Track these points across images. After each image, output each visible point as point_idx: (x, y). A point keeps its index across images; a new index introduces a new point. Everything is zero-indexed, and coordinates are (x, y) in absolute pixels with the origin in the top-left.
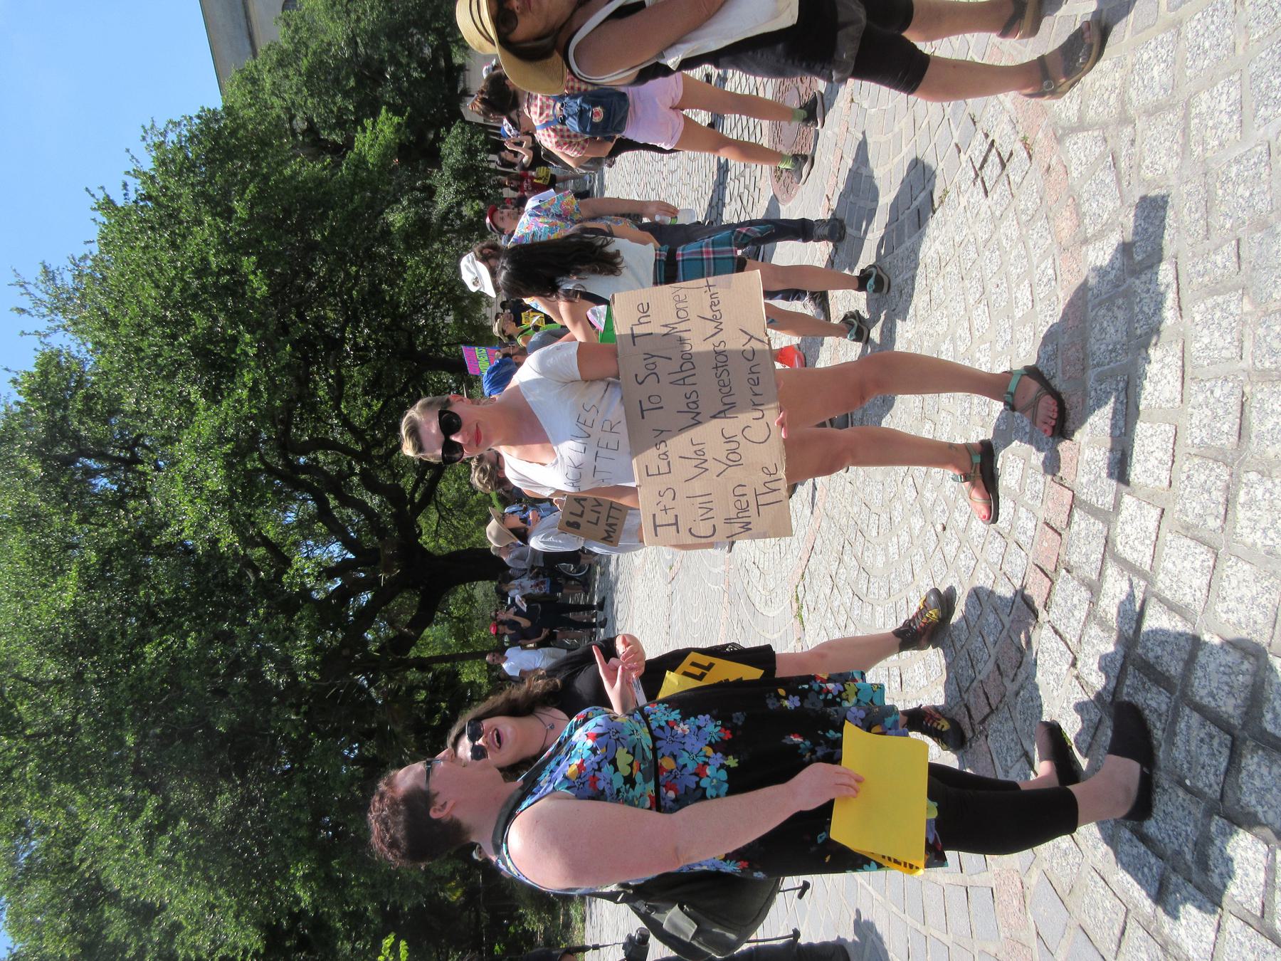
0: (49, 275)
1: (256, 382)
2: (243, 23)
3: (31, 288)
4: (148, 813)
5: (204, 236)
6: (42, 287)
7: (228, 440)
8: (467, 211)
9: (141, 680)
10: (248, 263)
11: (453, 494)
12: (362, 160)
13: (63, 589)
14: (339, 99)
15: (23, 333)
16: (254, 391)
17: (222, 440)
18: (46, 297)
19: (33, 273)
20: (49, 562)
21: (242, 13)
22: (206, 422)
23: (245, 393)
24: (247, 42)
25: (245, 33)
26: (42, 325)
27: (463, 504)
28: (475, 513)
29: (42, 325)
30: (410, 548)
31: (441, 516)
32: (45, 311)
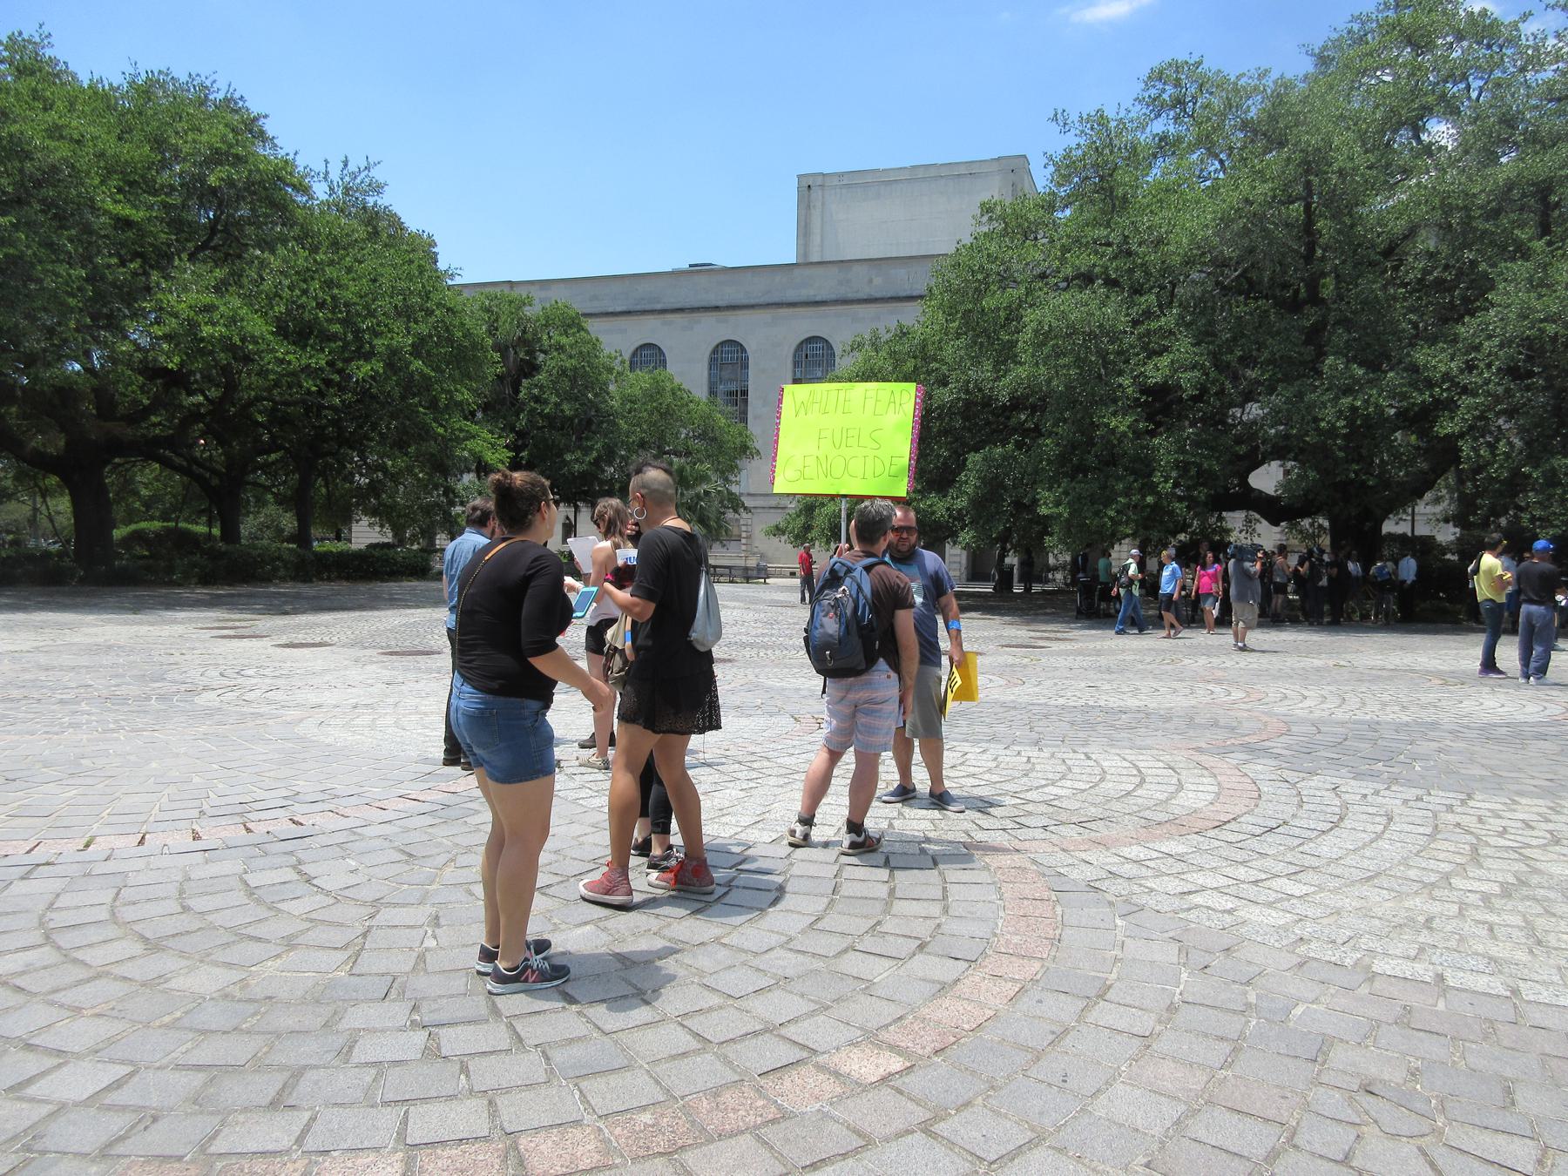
1: (289, 363)
2: (639, 308)
10: (380, 367)
14: (554, 399)
15: (326, 162)
16: (282, 361)
17: (243, 340)
18: (358, 181)
19: (378, 174)
21: (648, 307)
22: (258, 326)
24: (624, 308)
25: (631, 308)
26: (335, 176)
29: (335, 176)
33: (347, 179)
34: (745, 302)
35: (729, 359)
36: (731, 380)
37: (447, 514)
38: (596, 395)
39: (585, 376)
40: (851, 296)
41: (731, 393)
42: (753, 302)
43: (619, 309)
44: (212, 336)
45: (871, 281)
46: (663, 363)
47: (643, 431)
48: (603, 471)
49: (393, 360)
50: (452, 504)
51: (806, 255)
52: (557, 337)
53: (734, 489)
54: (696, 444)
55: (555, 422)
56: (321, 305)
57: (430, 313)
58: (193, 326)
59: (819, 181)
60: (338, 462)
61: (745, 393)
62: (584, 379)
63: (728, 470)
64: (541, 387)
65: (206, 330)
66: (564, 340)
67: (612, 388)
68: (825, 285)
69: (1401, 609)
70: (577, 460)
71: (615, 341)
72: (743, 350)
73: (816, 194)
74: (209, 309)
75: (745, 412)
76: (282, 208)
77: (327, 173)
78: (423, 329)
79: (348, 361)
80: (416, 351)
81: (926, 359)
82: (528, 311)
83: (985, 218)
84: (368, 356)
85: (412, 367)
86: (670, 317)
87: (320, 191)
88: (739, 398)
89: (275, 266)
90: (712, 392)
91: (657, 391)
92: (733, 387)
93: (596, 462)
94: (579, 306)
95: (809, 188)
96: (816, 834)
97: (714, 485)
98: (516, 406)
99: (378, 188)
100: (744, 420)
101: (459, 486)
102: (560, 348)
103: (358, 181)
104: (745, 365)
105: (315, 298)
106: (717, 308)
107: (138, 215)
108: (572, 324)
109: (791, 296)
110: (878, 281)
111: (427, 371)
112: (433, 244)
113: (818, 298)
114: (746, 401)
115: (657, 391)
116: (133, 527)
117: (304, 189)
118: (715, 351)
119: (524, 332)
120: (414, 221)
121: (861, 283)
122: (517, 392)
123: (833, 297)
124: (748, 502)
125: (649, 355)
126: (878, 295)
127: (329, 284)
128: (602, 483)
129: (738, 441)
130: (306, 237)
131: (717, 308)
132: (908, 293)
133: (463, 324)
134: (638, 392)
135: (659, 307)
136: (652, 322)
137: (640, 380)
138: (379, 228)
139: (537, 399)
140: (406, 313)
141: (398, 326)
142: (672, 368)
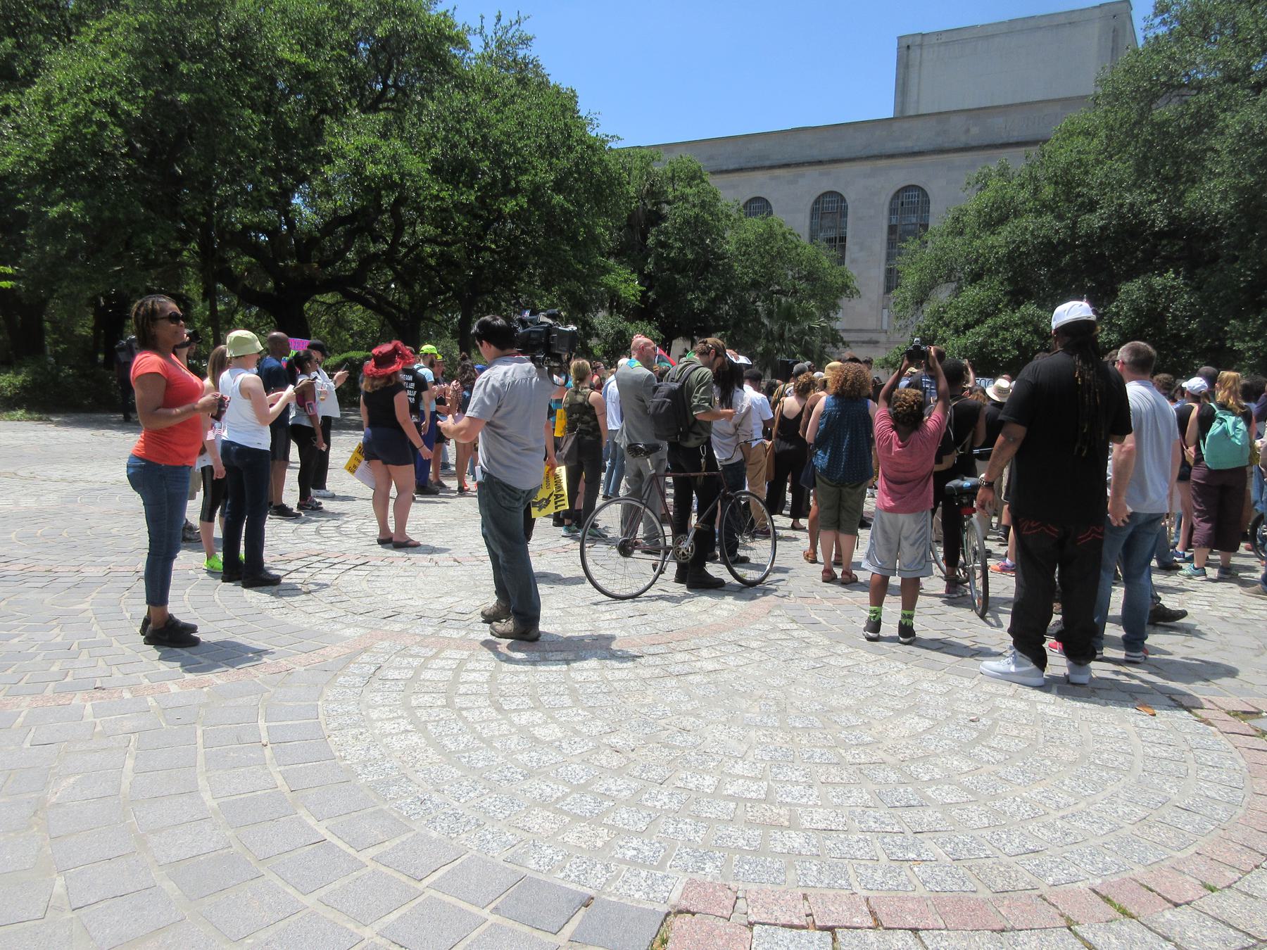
0: (526, 41)
1: (443, 199)
2: (749, 165)
3: (514, 28)
4: (125, 106)
5: (543, 173)
6: (517, 34)
7: (401, 179)
8: (593, 342)
9: (227, 106)
10: (524, 201)
11: (350, 316)
12: (606, 270)
13: (292, 51)
14: (678, 244)
15: (482, 17)
16: (437, 198)
17: (402, 176)
18: (510, 35)
19: (527, 29)
20: (313, 38)
21: (758, 164)
22: (415, 165)
23: (435, 192)
24: (737, 166)
25: (743, 165)
26: (489, 31)
27: (341, 326)
28: (333, 336)
29: (489, 31)
30: (312, 287)
31: (330, 306)
32: (500, 33)
33: (500, 33)
34: (847, 156)
35: (830, 210)
36: (830, 228)
37: (584, 345)
38: (713, 241)
39: (705, 223)
40: (947, 145)
41: (830, 240)
42: (853, 155)
43: (732, 167)
44: (375, 175)
45: (968, 131)
46: (770, 213)
47: (755, 273)
48: (720, 308)
49: (536, 193)
50: (589, 336)
51: (902, 111)
52: (681, 188)
53: (837, 325)
54: (802, 285)
55: (678, 266)
56: (473, 144)
57: (570, 149)
58: (358, 170)
59: (918, 40)
60: (495, 299)
61: (843, 239)
62: (701, 227)
63: (829, 308)
64: (666, 233)
65: (370, 169)
66: (688, 191)
67: (728, 234)
68: (922, 136)
69: (41, 332)
70: (697, 298)
71: (731, 193)
72: (843, 199)
73: (915, 54)
74: (372, 149)
75: (843, 258)
76: (443, 64)
77: (482, 27)
78: (563, 164)
79: (496, 197)
80: (559, 186)
81: (1069, 185)
82: (657, 168)
83: (1158, 20)
84: (514, 193)
85: (554, 202)
86: (778, 172)
87: (476, 44)
88: (839, 242)
89: (433, 108)
90: (812, 238)
91: (768, 237)
92: (832, 234)
93: (713, 301)
94: (698, 163)
95: (908, 49)
96: (883, 632)
97: (818, 322)
98: (644, 252)
99: (526, 41)
100: (841, 261)
101: (596, 321)
102: (684, 198)
103: (510, 35)
104: (843, 213)
105: (467, 137)
106: (820, 162)
107: (315, 66)
108: (694, 177)
109: (890, 147)
110: (975, 130)
111: (566, 205)
112: (573, 97)
113: (916, 149)
114: (843, 247)
115: (768, 237)
116: (344, 355)
117: (460, 42)
118: (817, 201)
119: (652, 185)
120: (559, 74)
121: (958, 132)
122: (645, 238)
123: (931, 147)
124: (846, 337)
125: (758, 206)
126: (974, 144)
127: (480, 124)
128: (717, 319)
129: (840, 281)
130: (463, 83)
131: (820, 162)
132: (1005, 140)
133: (601, 160)
134: (752, 237)
135: (767, 163)
136: (760, 176)
137: (753, 226)
138: (527, 77)
139: (663, 245)
140: (549, 151)
141: (541, 165)
142: (778, 215)
